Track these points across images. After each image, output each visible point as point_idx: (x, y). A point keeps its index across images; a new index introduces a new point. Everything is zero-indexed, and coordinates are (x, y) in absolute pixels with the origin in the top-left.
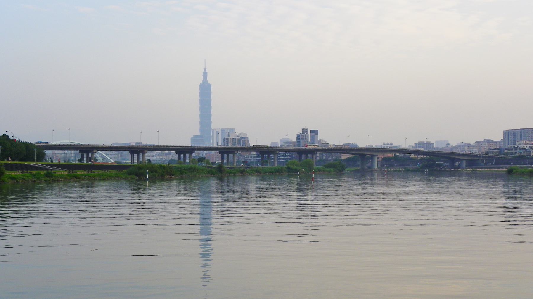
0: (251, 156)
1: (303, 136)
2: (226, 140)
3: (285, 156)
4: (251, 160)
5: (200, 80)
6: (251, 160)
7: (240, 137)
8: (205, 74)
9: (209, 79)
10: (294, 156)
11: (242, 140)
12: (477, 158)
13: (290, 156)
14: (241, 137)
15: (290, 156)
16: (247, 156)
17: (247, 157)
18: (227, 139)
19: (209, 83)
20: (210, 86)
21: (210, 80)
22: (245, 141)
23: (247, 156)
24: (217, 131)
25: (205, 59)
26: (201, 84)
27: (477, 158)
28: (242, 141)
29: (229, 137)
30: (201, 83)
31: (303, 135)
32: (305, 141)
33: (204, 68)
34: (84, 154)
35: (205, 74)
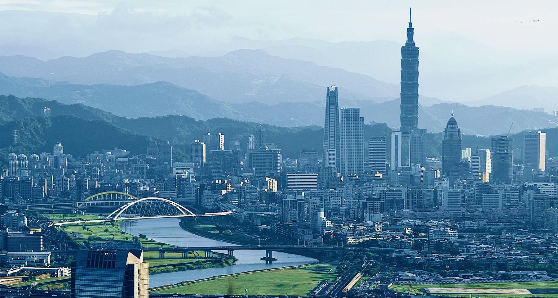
5: (403, 40)
7: (297, 199)
8: (410, 31)
9: (415, 39)
14: (298, 199)
21: (418, 41)
24: (396, 135)
25: (411, 8)
35: (410, 31)
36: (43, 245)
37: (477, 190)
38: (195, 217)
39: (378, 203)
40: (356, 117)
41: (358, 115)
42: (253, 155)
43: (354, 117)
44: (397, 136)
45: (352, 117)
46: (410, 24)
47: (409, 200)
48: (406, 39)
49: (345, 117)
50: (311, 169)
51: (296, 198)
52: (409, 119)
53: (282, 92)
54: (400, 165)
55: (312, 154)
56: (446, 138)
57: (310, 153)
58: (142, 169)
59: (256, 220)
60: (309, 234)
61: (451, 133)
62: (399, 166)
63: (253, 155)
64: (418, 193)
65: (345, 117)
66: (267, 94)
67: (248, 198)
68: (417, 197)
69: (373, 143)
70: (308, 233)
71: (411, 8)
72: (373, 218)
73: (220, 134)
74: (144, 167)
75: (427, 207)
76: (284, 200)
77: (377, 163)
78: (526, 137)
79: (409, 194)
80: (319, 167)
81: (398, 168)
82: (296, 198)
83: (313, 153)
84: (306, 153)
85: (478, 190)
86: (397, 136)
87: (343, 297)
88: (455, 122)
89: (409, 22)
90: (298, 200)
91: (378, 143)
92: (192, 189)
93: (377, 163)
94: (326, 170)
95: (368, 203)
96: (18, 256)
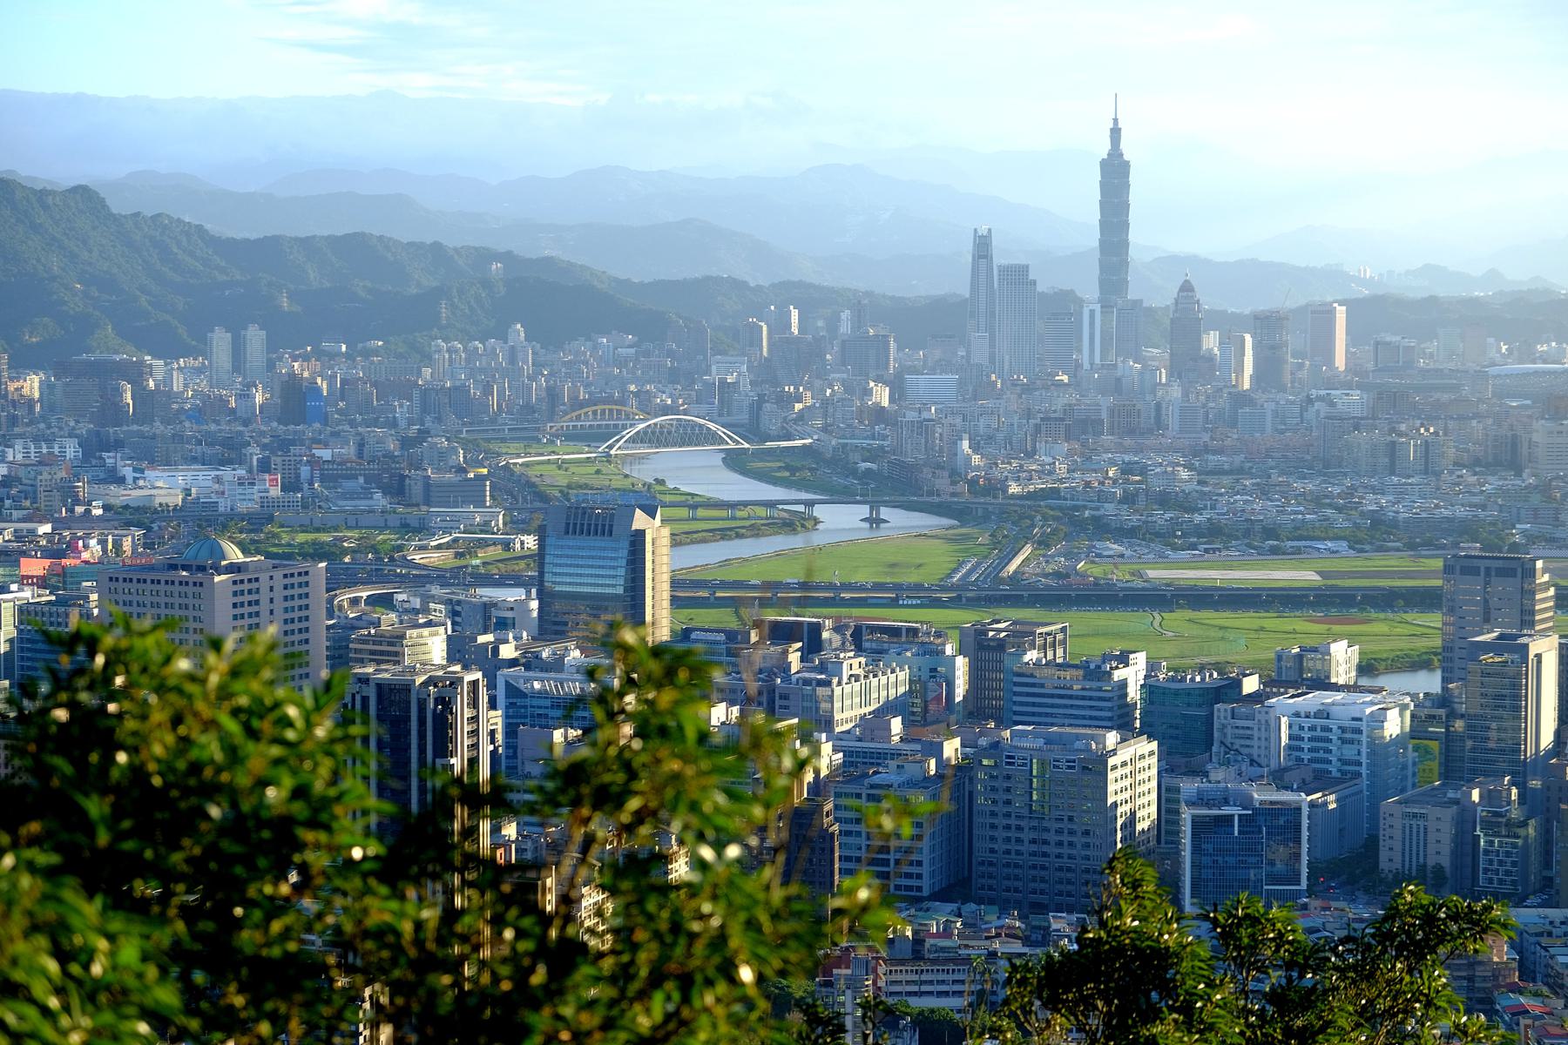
8: (1116, 133)
20: (1126, 166)
21: (1128, 150)
35: (1116, 133)
44: (1092, 312)
46: (1116, 120)
56: (1177, 315)
86: (1092, 312)
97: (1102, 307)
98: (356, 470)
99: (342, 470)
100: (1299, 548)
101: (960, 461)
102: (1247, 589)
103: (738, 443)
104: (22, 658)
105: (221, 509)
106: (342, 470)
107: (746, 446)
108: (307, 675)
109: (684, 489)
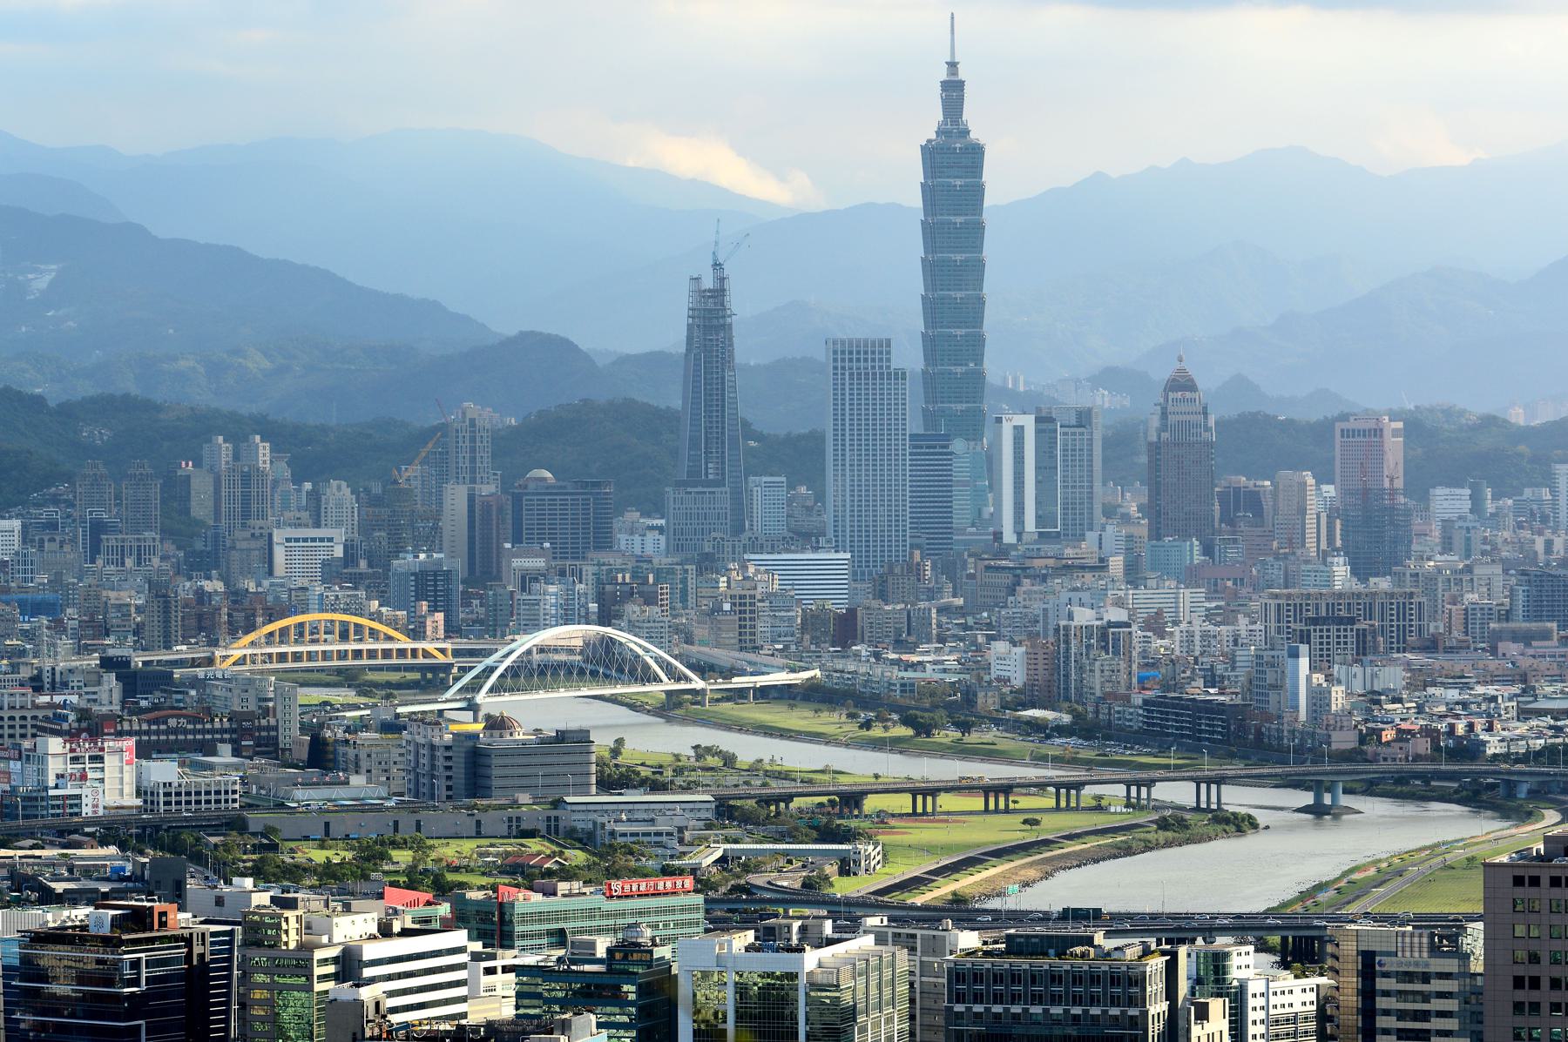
0: (1131, 710)
1: (1273, 657)
2: (1062, 632)
3: (1213, 726)
4: (1131, 720)
5: (928, 122)
6: (1131, 720)
7: (1105, 620)
8: (953, 91)
9: (970, 115)
10: (1232, 728)
11: (1112, 630)
12: (1551, 779)
13: (1223, 728)
14: (1109, 622)
15: (1223, 728)
16: (1120, 709)
17: (1119, 712)
18: (1066, 628)
19: (972, 135)
20: (975, 154)
21: (978, 122)
22: (1119, 633)
23: (1120, 709)
24: (1015, 427)
25: (952, 14)
26: (929, 141)
27: (1551, 779)
28: (1113, 634)
29: (1073, 624)
30: (934, 136)
31: (1272, 653)
32: (1276, 672)
33: (944, 77)
34: (1092, 1016)
35: (953, 91)
36: (597, 784)
37: (1524, 591)
38: (703, 691)
39: (1349, 633)
40: (873, 367)
41: (889, 360)
42: (524, 498)
43: (873, 367)
44: (1019, 431)
45: (859, 368)
46: (953, 65)
47: (1422, 623)
48: (937, 115)
49: (843, 368)
50: (726, 543)
51: (1102, 619)
52: (956, 378)
53: (71, 324)
54: (1030, 525)
55: (710, 493)
56: (1165, 436)
57: (705, 493)
58: (139, 550)
59: (983, 694)
60: (1342, 727)
61: (1180, 418)
62: (1026, 530)
63: (527, 500)
64: (1401, 600)
65: (843, 368)
66: (24, 329)
67: (766, 629)
68: (1365, 615)
69: (936, 454)
70: (1339, 724)
71: (952, 14)
72: (1375, 681)
73: (258, 438)
74: (147, 544)
75: (1451, 648)
76: (1064, 627)
77: (923, 523)
78: (1342, 436)
79: (1370, 604)
80: (750, 538)
81: (1025, 537)
82: (1102, 619)
83: (714, 493)
84: (689, 490)
85: (1528, 591)
86: (1019, 431)
87: (281, 1041)
88: (1190, 383)
89: (949, 60)
90: (1111, 624)
91: (927, 454)
92: (542, 604)
93: (923, 523)
94: (734, 546)
95: (1315, 631)
96: (622, 811)
97: (1037, 420)
98: (186, 732)
99: (158, 733)
100: (1415, 1019)
101: (716, 675)
102: (1045, 917)
103: (680, 678)
104: (731, 472)
105: (87, 811)
106: (158, 733)
107: (698, 683)
108: (377, 1004)
109: (771, 955)
